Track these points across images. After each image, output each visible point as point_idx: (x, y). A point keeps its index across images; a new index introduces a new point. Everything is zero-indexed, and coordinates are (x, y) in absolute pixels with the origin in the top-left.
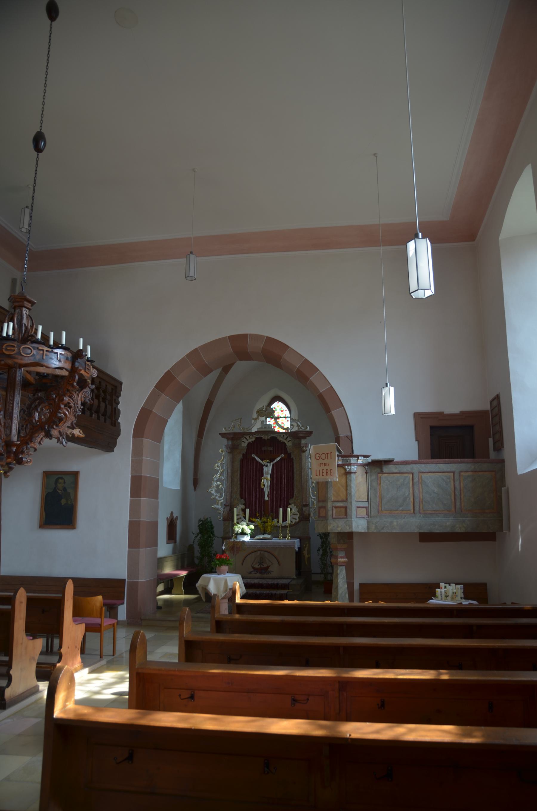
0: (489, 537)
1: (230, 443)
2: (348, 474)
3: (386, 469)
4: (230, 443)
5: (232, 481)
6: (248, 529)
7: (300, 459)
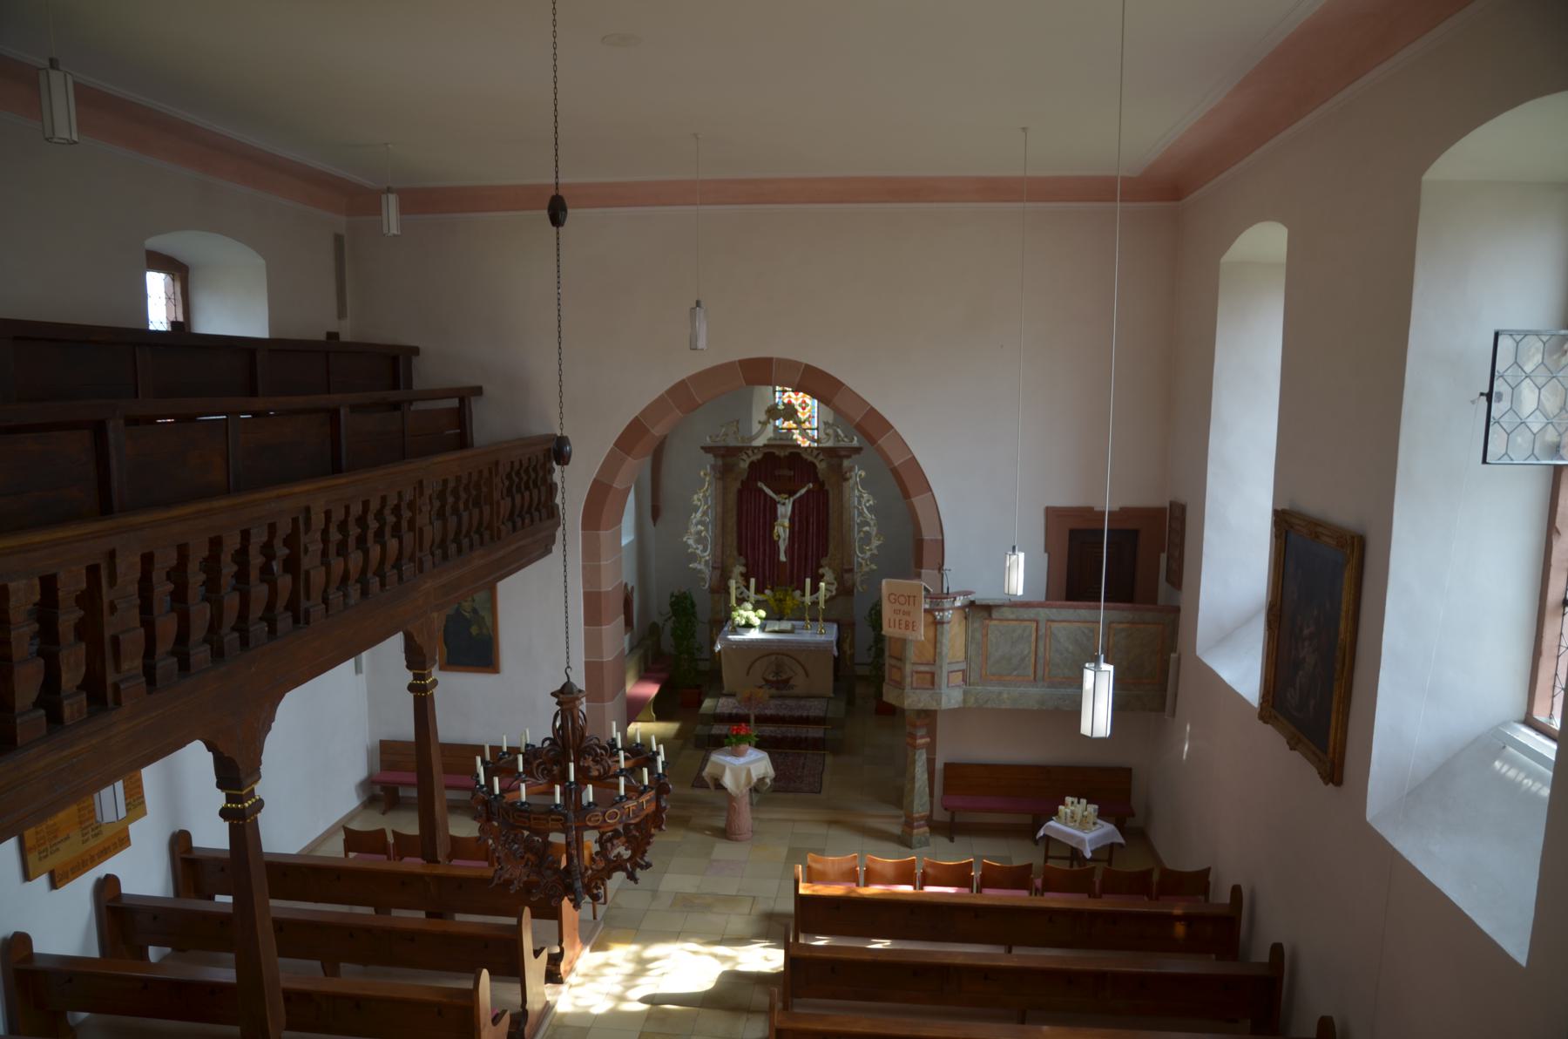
1: (720, 462)
2: (937, 624)
4: (720, 462)
5: (724, 526)
7: (841, 492)
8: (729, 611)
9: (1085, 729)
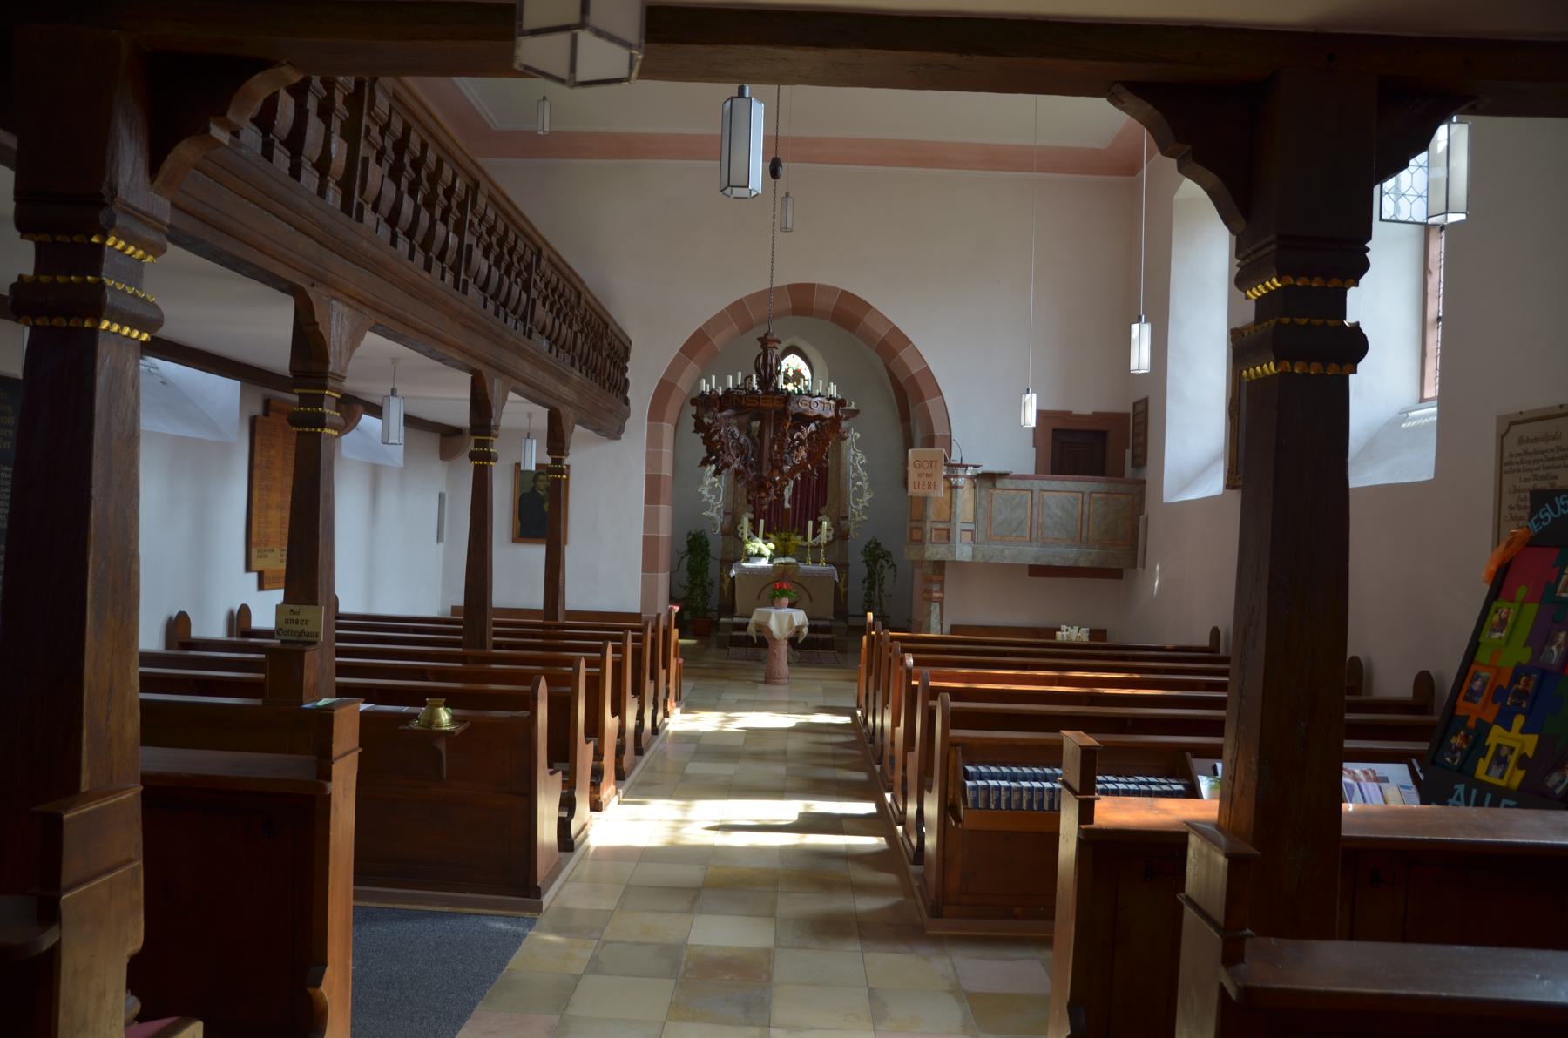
0: (1115, 574)
2: (953, 488)
3: (999, 484)
6: (767, 549)
7: (839, 451)
8: (742, 543)
9: (1134, 365)
